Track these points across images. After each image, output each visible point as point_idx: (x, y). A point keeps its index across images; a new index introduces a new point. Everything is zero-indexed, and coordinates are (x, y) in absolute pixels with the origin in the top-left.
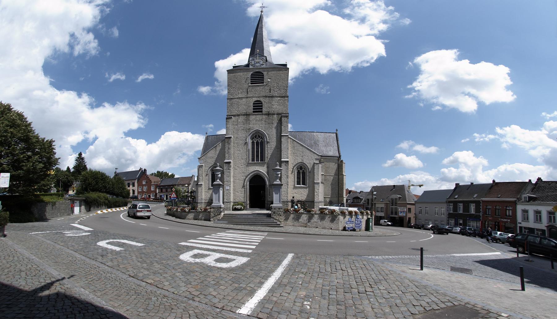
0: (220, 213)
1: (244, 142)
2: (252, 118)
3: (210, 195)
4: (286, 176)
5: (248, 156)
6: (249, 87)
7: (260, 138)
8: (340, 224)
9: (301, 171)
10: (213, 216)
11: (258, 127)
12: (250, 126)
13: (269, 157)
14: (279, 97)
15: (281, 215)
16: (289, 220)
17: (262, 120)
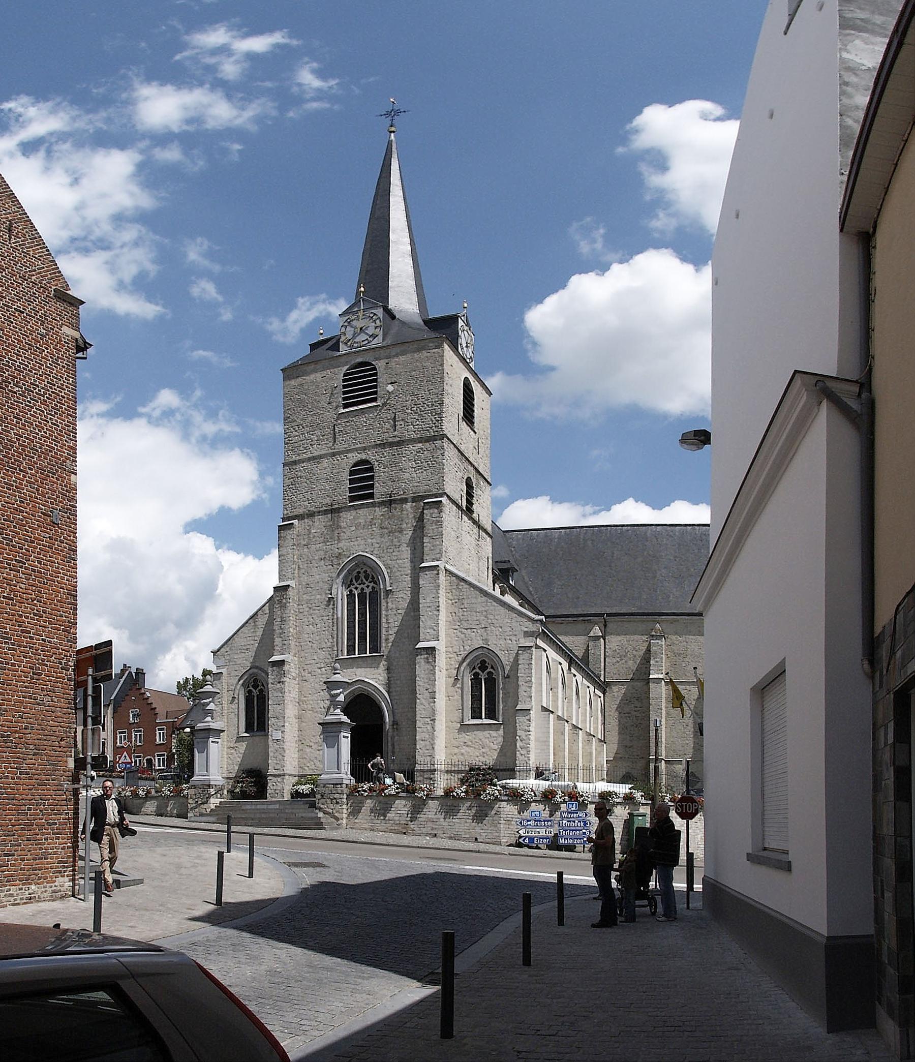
0: (207, 798)
1: (325, 598)
2: (347, 517)
3: (241, 756)
4: (428, 695)
5: (335, 640)
6: (338, 419)
7: (370, 579)
8: (502, 826)
9: (483, 676)
10: (194, 805)
11: (361, 547)
12: (340, 545)
13: (392, 638)
14: (420, 440)
15: (337, 803)
16: (360, 816)
17: (371, 523)
